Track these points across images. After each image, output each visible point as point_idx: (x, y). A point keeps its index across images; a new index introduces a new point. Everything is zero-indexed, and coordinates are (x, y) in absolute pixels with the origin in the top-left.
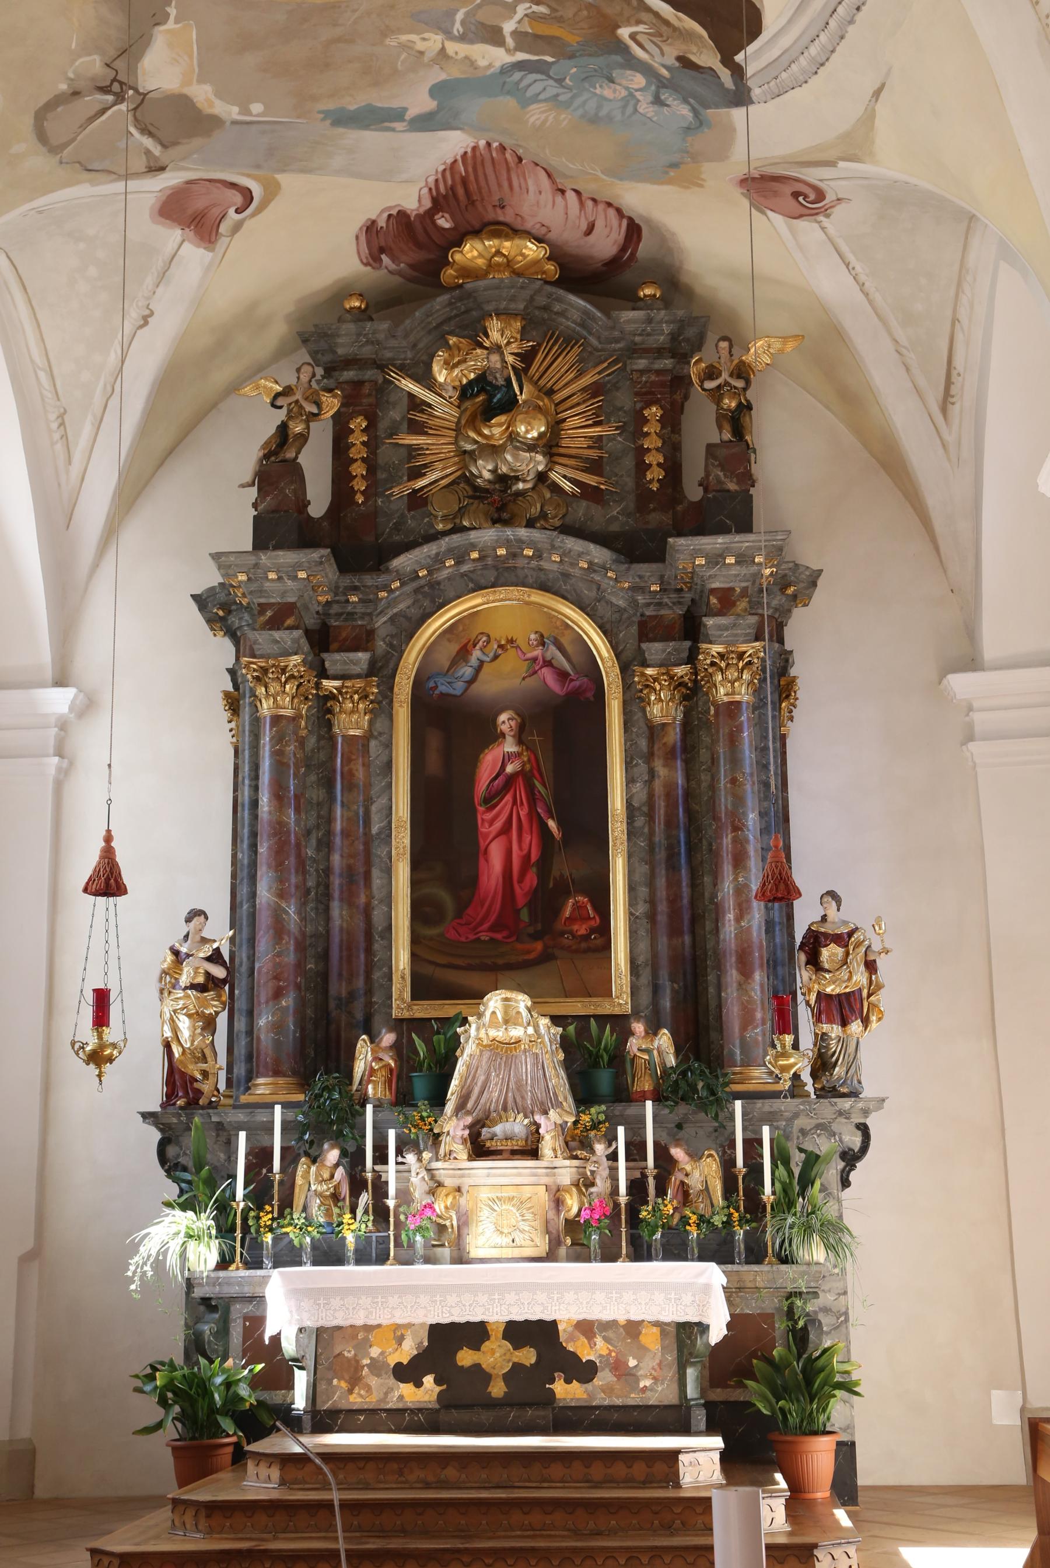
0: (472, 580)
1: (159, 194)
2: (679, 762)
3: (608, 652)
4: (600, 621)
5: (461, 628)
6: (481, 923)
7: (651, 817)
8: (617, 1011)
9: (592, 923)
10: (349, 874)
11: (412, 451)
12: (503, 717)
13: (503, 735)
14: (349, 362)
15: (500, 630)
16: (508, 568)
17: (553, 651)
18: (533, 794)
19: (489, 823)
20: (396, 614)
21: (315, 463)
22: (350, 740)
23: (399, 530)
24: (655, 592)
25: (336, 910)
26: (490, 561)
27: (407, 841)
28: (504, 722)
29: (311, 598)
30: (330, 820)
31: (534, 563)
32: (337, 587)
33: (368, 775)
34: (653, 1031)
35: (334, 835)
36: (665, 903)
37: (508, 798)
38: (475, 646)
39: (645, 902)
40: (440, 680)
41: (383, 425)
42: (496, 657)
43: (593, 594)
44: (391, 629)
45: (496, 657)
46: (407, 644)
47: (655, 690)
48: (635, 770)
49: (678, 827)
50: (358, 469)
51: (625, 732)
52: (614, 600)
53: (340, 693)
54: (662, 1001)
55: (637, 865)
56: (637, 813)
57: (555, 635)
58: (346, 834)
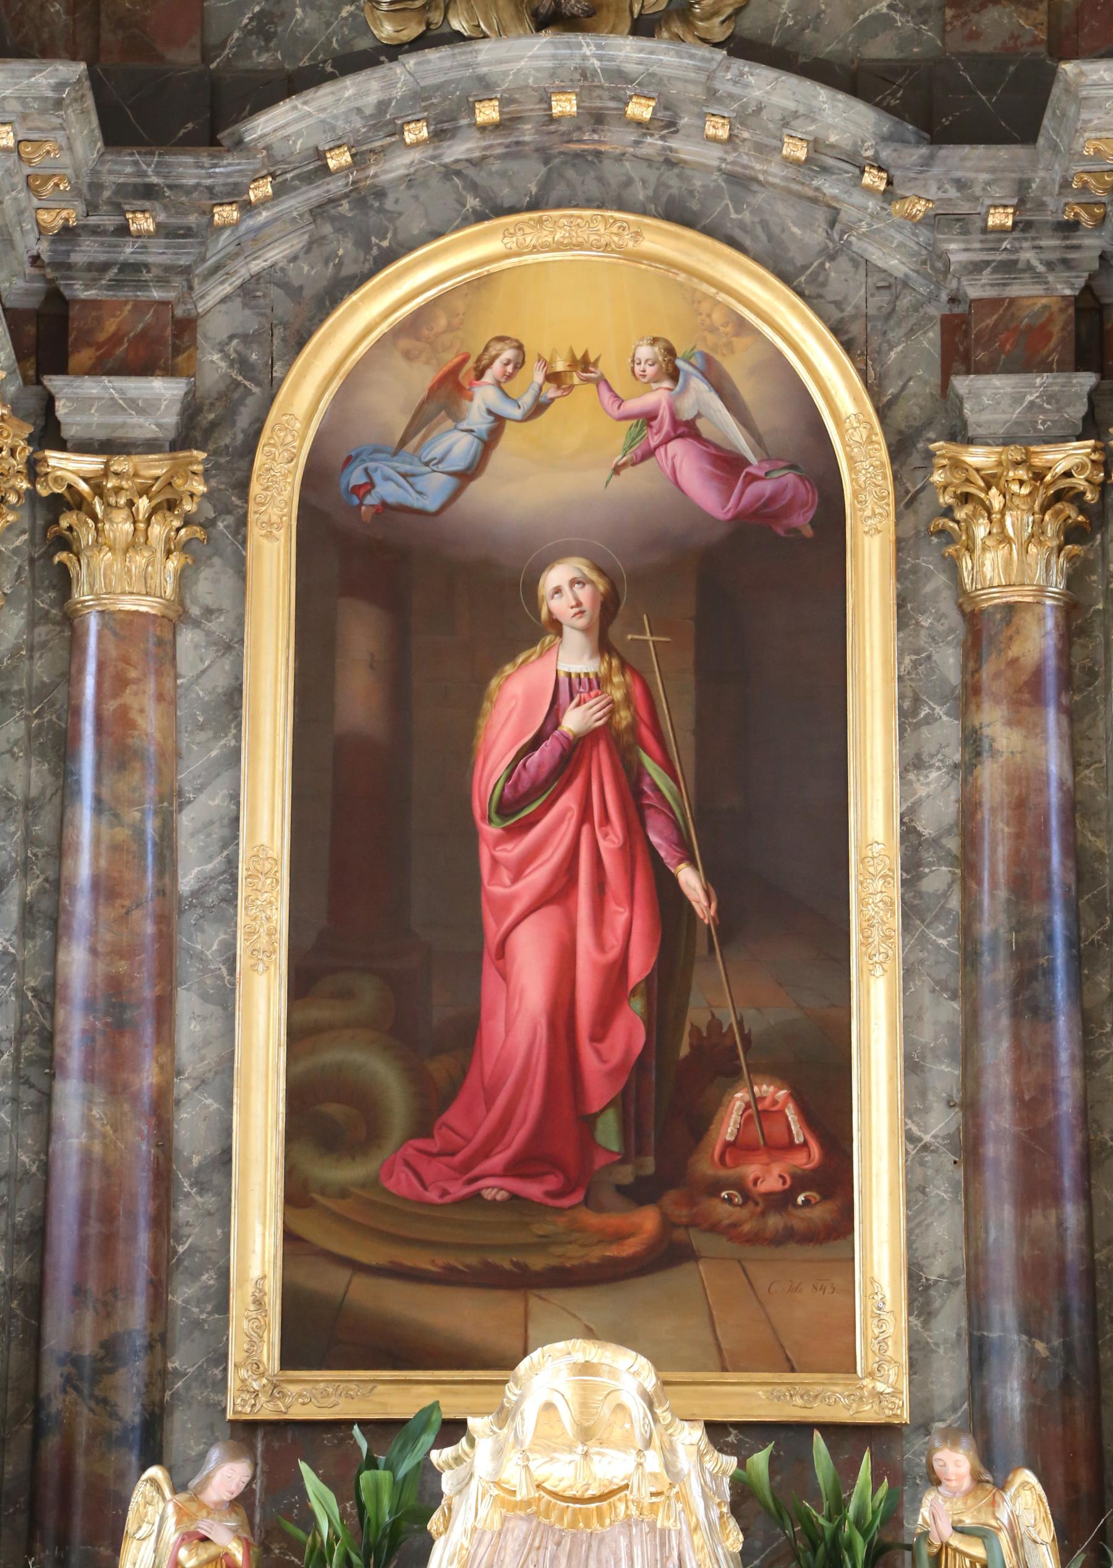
0: (474, 187)
2: (1051, 715)
3: (856, 400)
4: (836, 315)
5: (442, 322)
6: (485, 1151)
7: (968, 867)
8: (868, 1414)
9: (800, 1161)
10: (113, 1001)
12: (557, 576)
13: (556, 626)
15: (552, 338)
16: (578, 155)
17: (698, 397)
18: (639, 794)
19: (513, 870)
20: (257, 277)
22: (122, 626)
23: (268, 37)
24: (1002, 230)
25: (73, 1103)
26: (528, 133)
27: (280, 916)
28: (558, 590)
29: (20, 213)
30: (60, 849)
31: (653, 144)
32: (96, 187)
33: (173, 728)
34: (992, 1471)
35: (72, 891)
36: (1008, 1107)
37: (569, 801)
38: (480, 374)
39: (950, 1104)
40: (382, 468)
42: (539, 408)
43: (816, 237)
44: (244, 319)
45: (539, 408)
46: (289, 364)
47: (989, 511)
48: (925, 732)
49: (1047, 894)
51: (901, 625)
52: (876, 255)
53: (98, 490)
54: (997, 1390)
55: (927, 999)
56: (928, 855)
58: (106, 889)
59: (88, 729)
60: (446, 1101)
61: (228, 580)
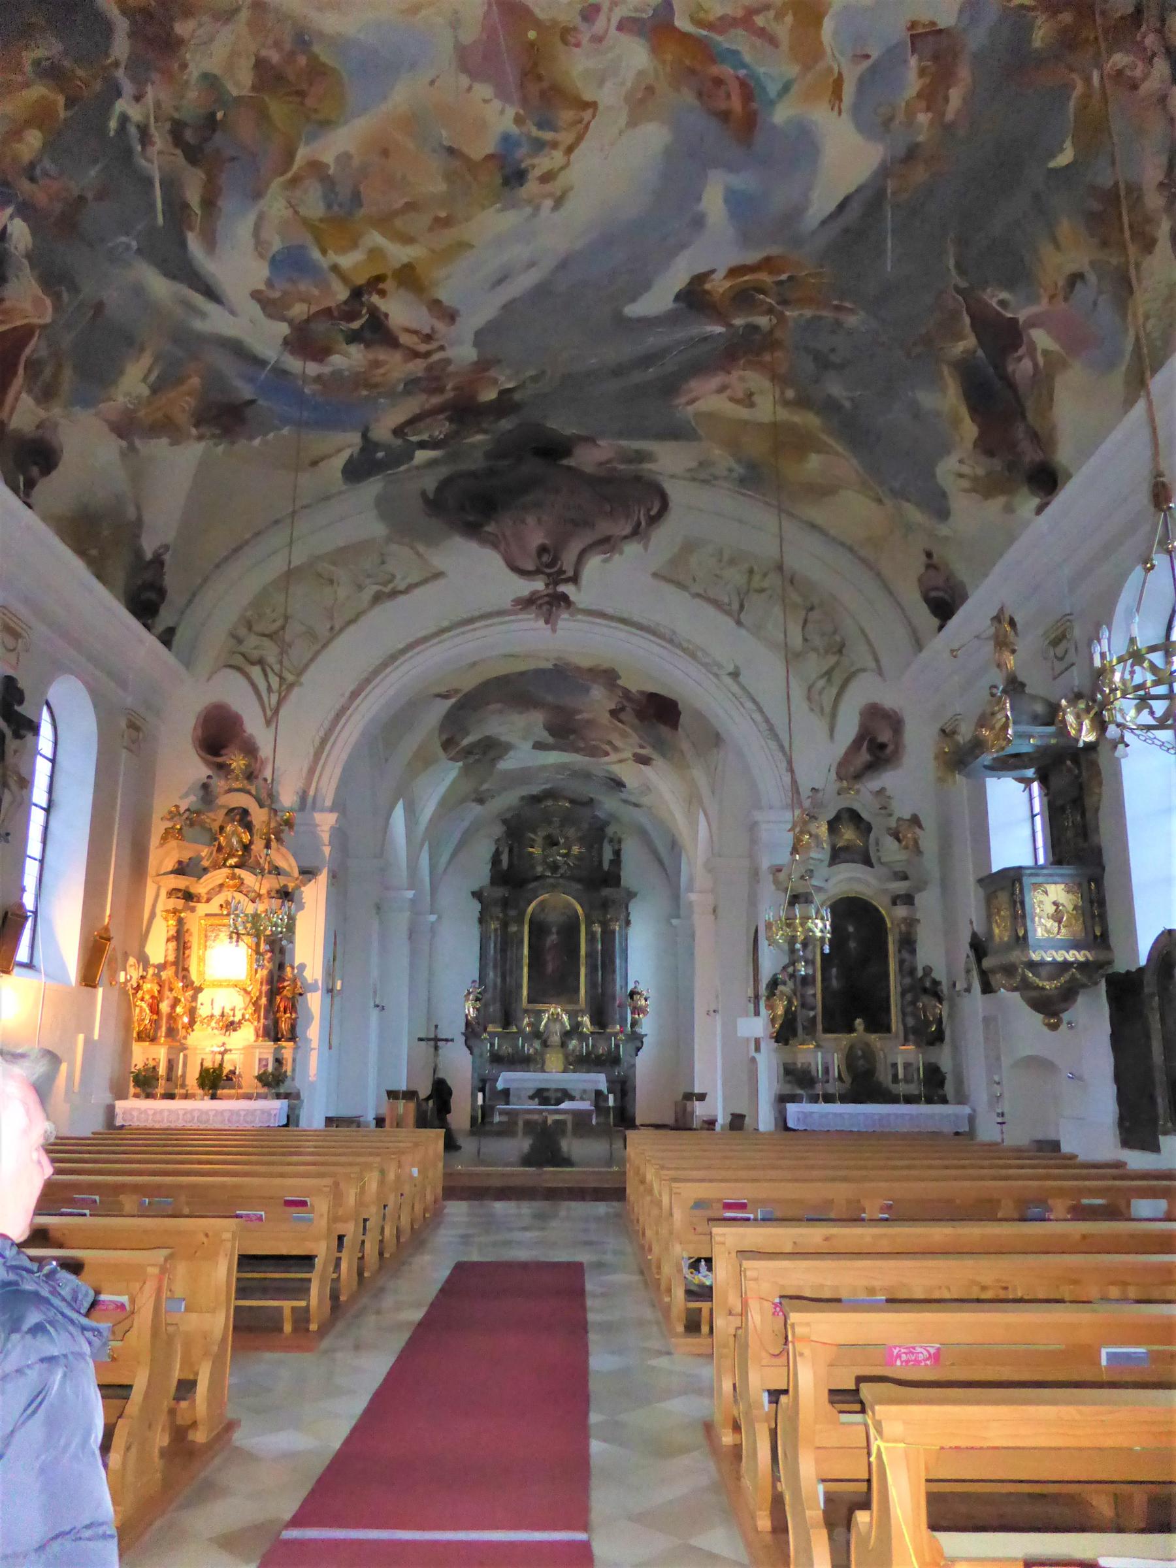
1: (421, 548)
21: (505, 858)
57: (569, 906)
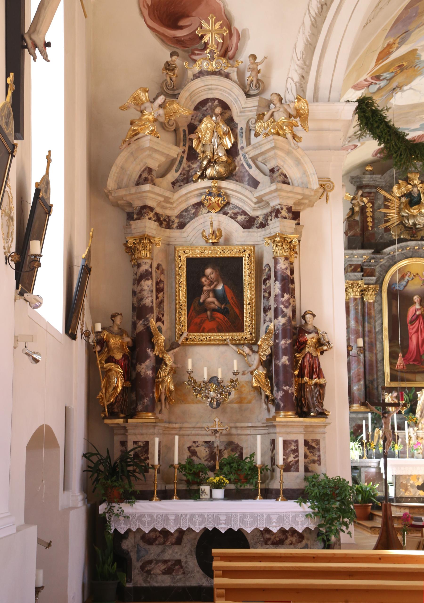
0: (404, 255)
6: (410, 359)
11: (385, 214)
12: (415, 297)
13: (415, 303)
14: (367, 186)
15: (414, 272)
22: (370, 303)
37: (417, 322)
38: (406, 275)
41: (376, 205)
42: (413, 279)
45: (413, 279)
50: (369, 219)
59: (366, 314)
60: (406, 354)
61: (380, 298)
